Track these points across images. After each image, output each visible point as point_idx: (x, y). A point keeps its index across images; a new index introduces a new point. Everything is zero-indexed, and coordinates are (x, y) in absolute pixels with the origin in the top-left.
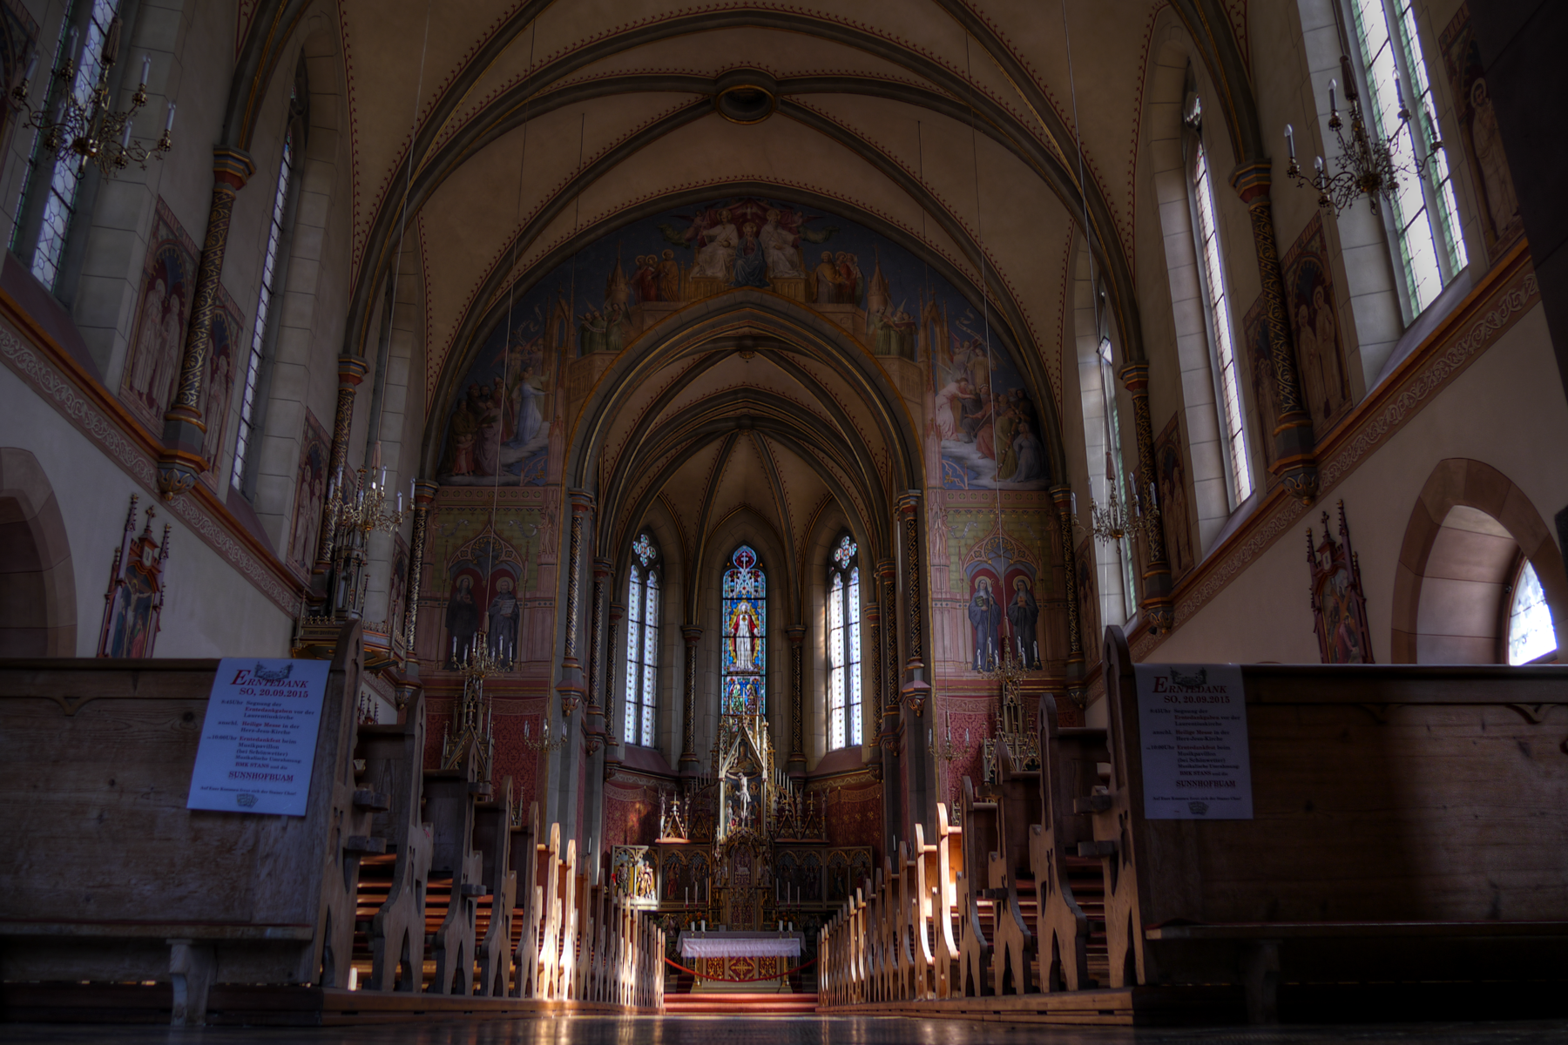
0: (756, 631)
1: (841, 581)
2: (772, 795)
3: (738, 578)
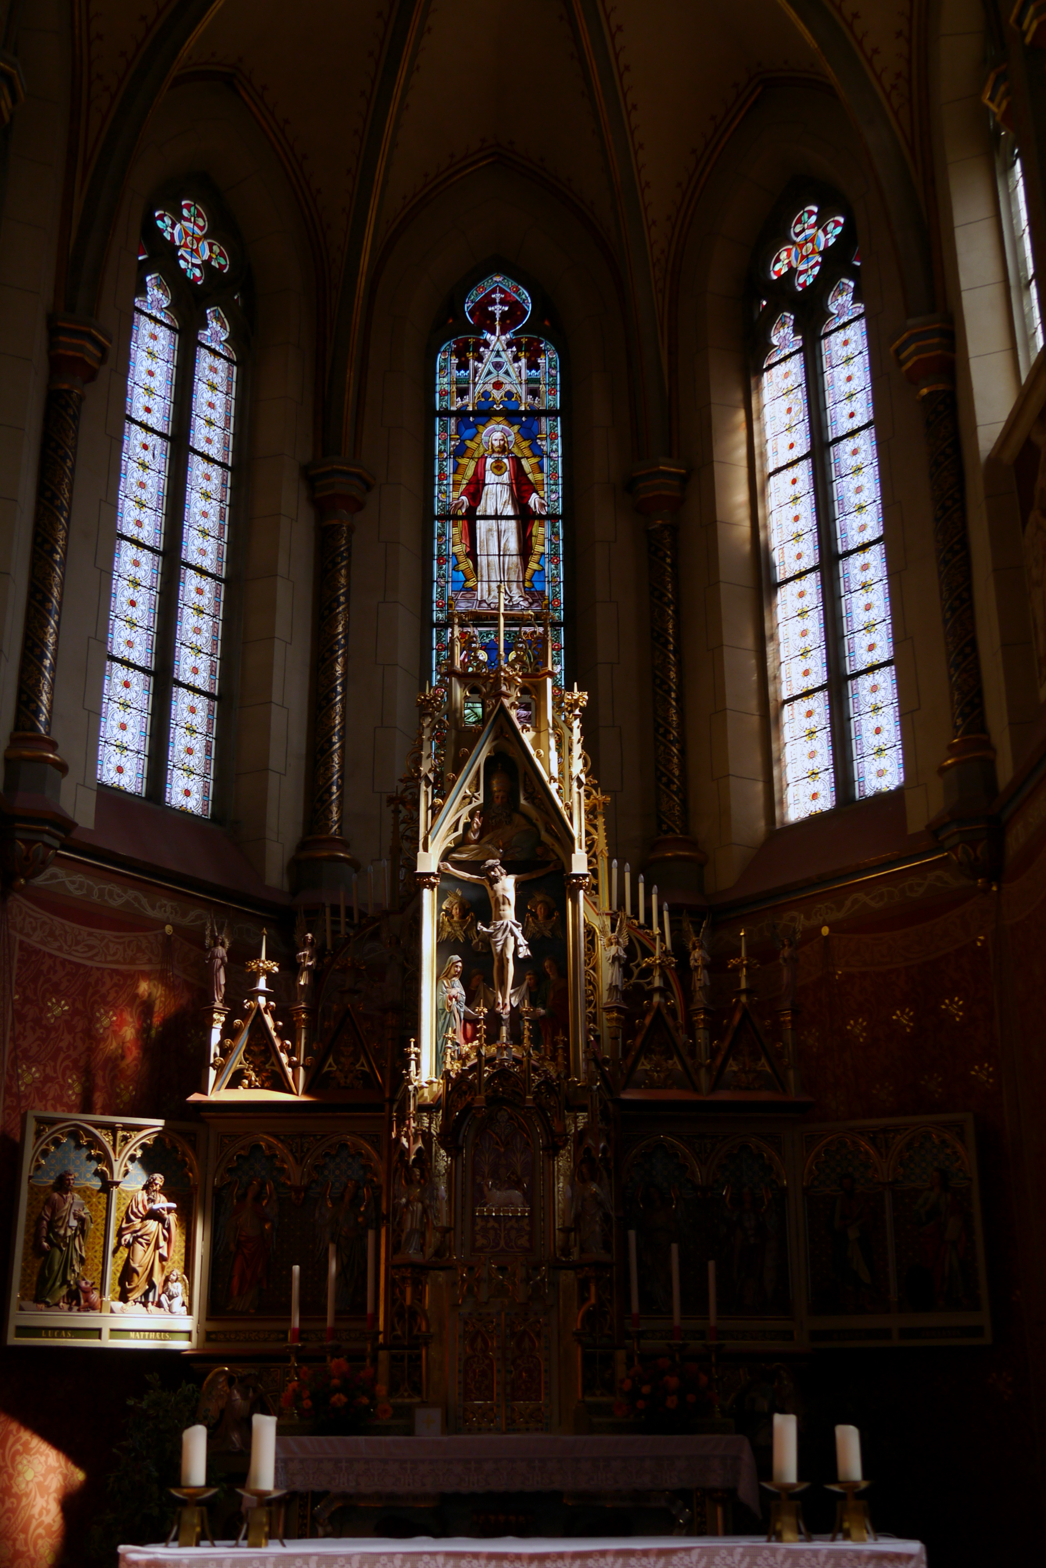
0: (534, 500)
1: (796, 332)
2: (601, 942)
3: (480, 359)
